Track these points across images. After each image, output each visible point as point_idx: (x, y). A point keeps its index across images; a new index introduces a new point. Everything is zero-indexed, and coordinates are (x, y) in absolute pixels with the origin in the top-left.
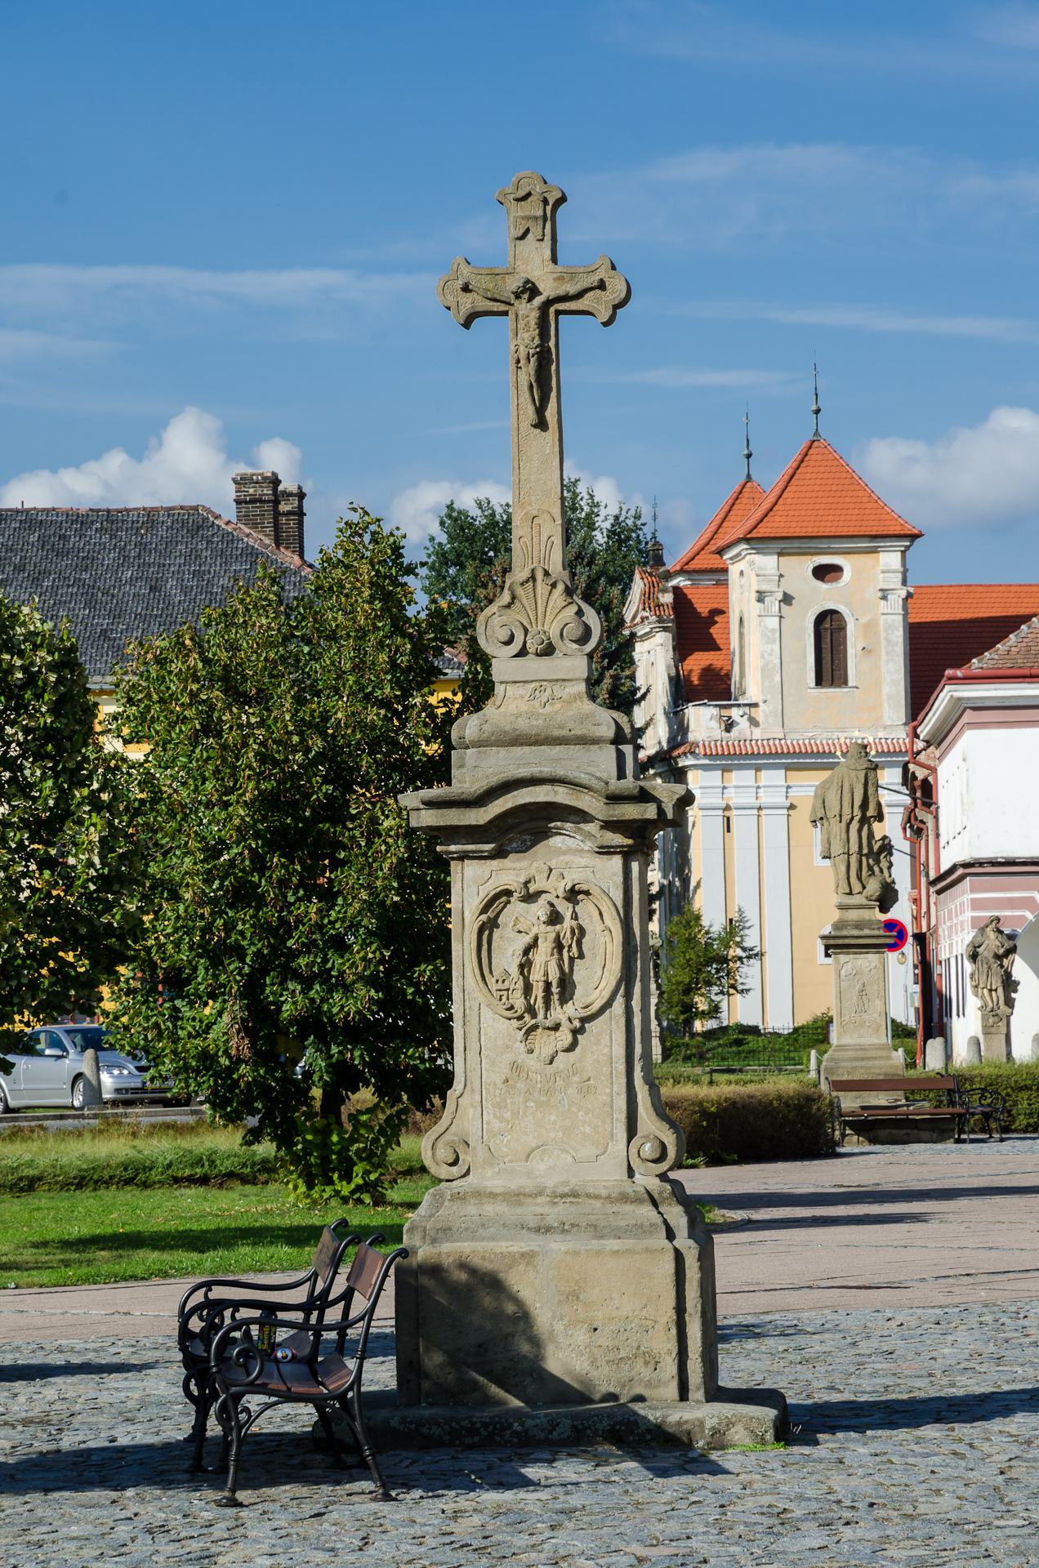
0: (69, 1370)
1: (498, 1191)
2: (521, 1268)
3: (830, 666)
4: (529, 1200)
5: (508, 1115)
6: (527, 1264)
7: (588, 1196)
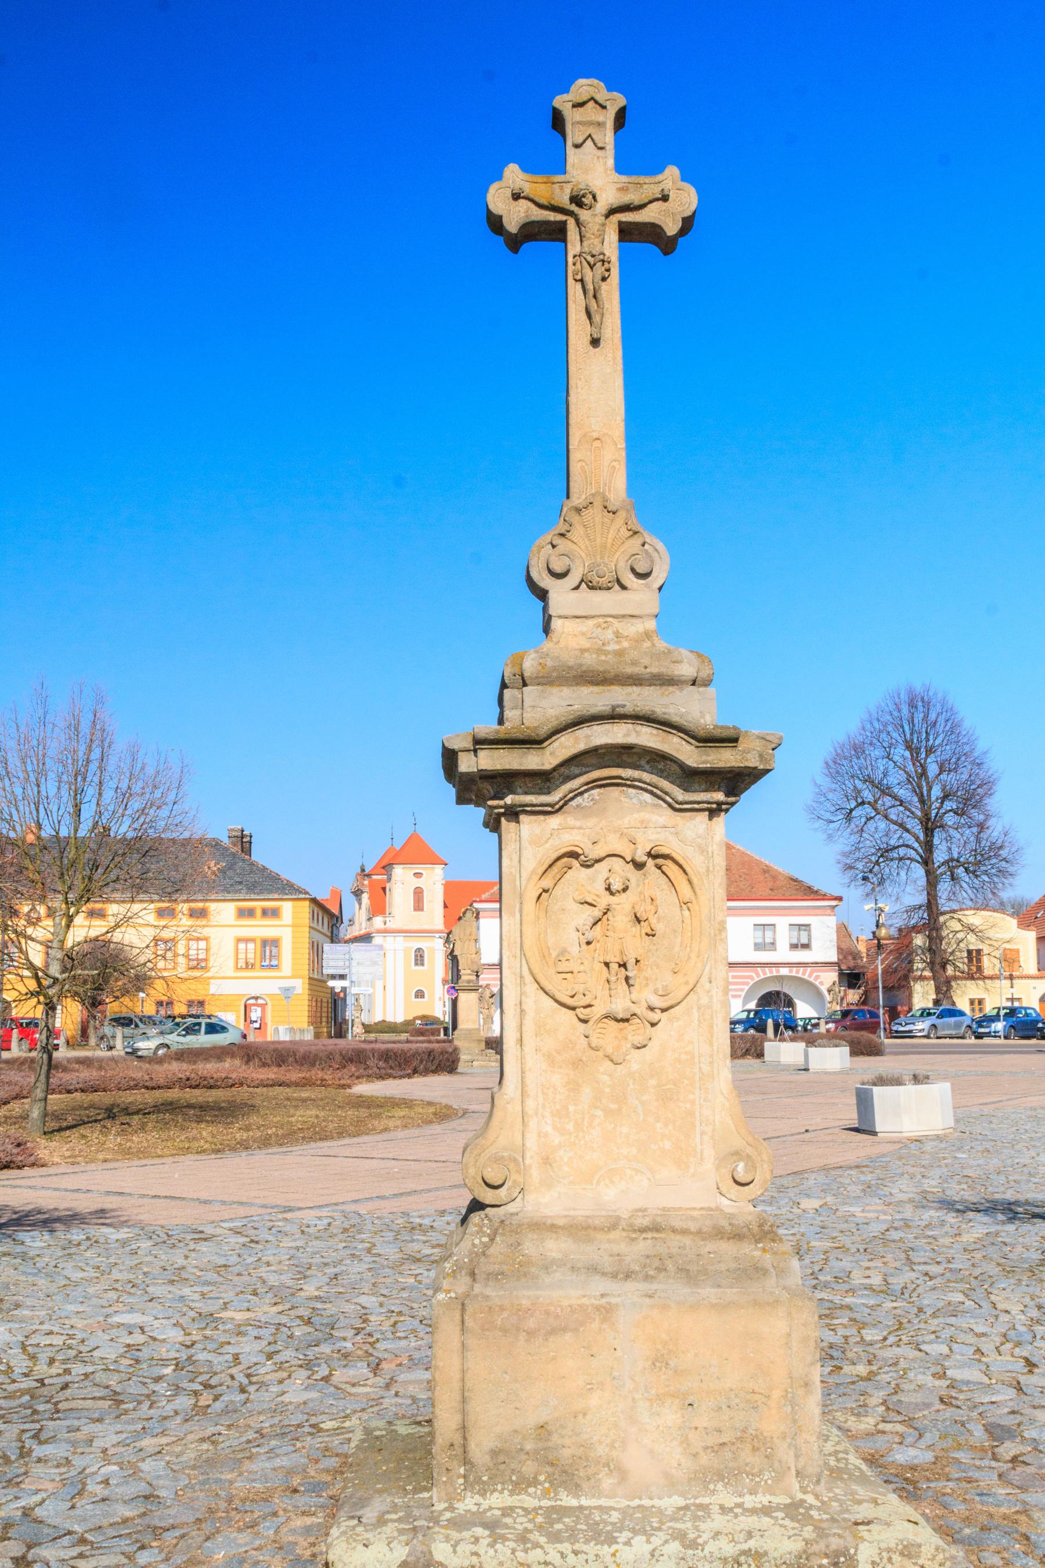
0: (651, 202)
1: (561, 1222)
2: (595, 1325)
3: (419, 906)
4: (600, 1236)
5: (570, 1126)
6: (604, 1320)
7: (674, 1231)
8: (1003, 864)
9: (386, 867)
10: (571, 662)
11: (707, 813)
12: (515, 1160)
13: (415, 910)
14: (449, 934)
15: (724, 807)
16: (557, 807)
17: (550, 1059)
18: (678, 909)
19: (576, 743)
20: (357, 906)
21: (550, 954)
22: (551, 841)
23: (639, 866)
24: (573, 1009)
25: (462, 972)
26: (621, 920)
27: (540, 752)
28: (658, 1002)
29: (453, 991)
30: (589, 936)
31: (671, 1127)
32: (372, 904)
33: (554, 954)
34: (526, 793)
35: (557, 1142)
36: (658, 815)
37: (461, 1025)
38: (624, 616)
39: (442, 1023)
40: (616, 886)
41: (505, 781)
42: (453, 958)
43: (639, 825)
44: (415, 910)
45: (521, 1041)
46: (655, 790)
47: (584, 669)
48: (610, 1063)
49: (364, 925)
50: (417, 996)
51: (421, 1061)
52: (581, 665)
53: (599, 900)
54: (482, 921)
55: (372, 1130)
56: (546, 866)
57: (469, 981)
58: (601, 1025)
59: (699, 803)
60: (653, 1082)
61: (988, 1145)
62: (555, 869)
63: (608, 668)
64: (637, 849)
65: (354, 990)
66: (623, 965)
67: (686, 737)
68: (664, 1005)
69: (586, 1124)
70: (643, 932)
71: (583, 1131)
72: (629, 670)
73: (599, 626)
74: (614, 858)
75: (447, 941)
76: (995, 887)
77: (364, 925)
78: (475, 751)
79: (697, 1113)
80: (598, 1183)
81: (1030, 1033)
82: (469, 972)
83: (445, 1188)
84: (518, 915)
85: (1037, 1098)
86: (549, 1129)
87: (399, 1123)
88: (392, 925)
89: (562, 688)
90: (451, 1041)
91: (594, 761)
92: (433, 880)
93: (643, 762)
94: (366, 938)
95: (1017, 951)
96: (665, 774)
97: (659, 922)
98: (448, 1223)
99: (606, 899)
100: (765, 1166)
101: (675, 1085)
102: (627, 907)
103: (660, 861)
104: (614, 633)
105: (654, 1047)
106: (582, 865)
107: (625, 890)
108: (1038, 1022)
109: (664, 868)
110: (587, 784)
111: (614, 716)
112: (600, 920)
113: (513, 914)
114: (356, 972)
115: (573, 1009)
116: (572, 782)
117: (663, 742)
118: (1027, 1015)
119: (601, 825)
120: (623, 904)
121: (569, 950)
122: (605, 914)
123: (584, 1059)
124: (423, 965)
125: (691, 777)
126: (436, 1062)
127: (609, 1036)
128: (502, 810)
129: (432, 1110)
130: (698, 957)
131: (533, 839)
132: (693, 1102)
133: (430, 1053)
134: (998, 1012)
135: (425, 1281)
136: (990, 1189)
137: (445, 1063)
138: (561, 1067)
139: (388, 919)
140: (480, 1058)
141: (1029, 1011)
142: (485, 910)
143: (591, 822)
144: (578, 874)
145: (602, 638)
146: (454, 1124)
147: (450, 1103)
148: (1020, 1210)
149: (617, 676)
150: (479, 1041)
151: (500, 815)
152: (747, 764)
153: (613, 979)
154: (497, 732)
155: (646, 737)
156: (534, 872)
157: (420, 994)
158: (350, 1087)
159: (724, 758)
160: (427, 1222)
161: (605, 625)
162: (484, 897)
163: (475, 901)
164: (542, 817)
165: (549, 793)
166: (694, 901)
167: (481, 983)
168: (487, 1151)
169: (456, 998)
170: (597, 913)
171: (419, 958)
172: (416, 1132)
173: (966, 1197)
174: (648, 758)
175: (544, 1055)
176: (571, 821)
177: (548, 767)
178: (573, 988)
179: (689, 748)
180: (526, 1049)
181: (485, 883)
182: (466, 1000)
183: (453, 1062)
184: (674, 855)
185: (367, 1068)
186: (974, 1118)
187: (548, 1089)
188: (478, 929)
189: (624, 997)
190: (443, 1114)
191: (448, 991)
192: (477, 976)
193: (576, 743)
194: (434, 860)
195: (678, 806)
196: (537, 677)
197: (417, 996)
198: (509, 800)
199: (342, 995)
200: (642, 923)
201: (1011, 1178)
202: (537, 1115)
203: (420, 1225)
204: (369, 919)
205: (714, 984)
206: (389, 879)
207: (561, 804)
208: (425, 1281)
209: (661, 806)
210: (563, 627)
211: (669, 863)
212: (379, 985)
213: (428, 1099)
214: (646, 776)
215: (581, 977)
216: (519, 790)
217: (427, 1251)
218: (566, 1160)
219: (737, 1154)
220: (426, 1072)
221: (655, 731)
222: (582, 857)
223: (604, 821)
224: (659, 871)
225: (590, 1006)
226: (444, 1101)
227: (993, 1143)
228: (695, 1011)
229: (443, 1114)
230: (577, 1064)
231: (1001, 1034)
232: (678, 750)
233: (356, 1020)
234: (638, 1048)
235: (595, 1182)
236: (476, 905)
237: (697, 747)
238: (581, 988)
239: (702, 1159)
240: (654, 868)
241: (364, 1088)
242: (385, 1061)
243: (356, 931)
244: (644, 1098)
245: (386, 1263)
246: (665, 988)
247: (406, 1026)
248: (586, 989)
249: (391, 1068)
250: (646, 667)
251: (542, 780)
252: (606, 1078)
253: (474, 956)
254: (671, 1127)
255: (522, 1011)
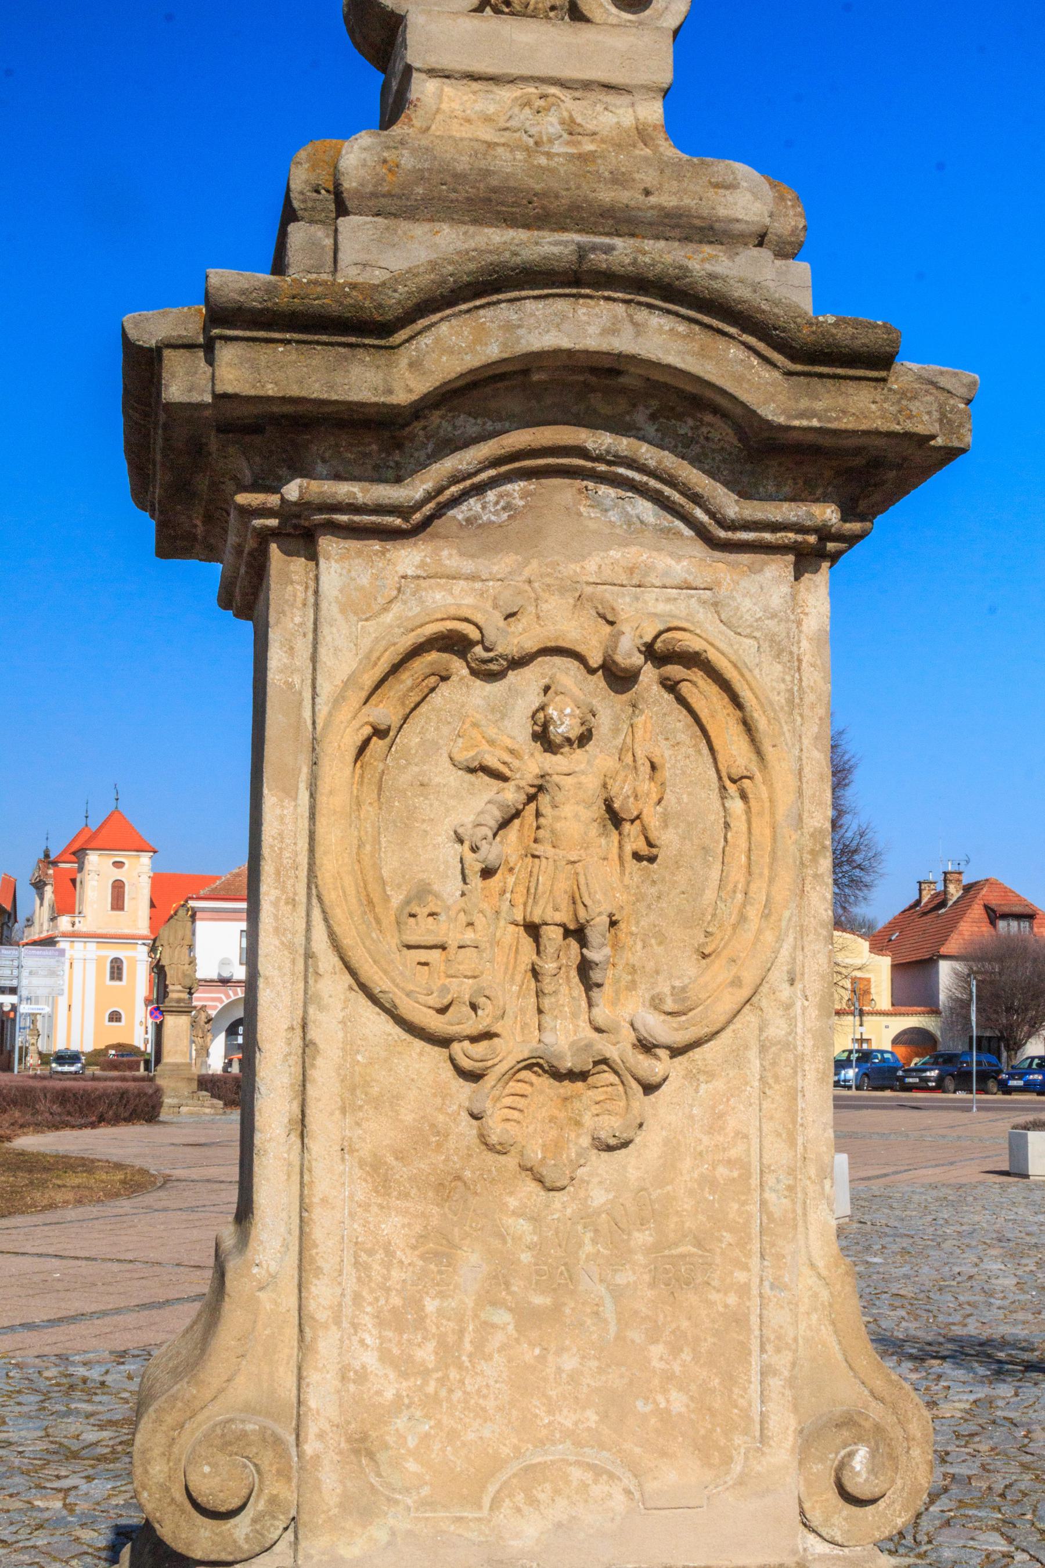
3: (118, 902)
5: (426, 1354)
8: (857, 872)
9: (79, 854)
10: (463, 164)
11: (791, 558)
12: (278, 1441)
13: (113, 909)
14: (155, 941)
15: (831, 546)
16: (417, 517)
17: (379, 1174)
18: (715, 795)
19: (477, 341)
20: (38, 902)
21: (387, 899)
22: (396, 608)
23: (619, 678)
24: (443, 1042)
25: (171, 988)
26: (573, 816)
27: (382, 358)
28: (660, 1028)
29: (157, 1013)
30: (491, 852)
31: (686, 1356)
32: (56, 901)
33: (397, 899)
34: (338, 477)
35: (389, 1395)
36: (671, 555)
37: (168, 1058)
38: (587, 85)
39: (143, 1053)
40: (565, 726)
41: (290, 432)
42: (159, 971)
43: (623, 579)
44: (113, 909)
45: (301, 1124)
46: (667, 491)
47: (494, 182)
48: (533, 1186)
49: (45, 927)
50: (111, 1019)
51: (110, 1106)
52: (487, 173)
53: (515, 763)
54: (199, 924)
55: (30, 1207)
56: (383, 666)
57: (179, 1001)
58: (514, 1086)
59: (774, 527)
60: (642, 1238)
61: (905, 1243)
62: (407, 678)
63: (555, 185)
64: (617, 636)
65: (24, 1008)
66: (578, 933)
67: (761, 346)
68: (679, 1038)
69: (468, 1347)
70: (628, 849)
71: (460, 1367)
72: (606, 195)
73: (528, 104)
74: (557, 660)
75: (153, 949)
76: (846, 901)
77: (45, 927)
78: (209, 348)
79: (754, 1320)
80: (496, 1504)
81: (886, 1083)
82: (179, 988)
83: (128, 1309)
84: (304, 796)
85: (930, 1171)
86: (370, 1359)
87: (70, 1196)
88: (81, 927)
89: (437, 226)
90: (151, 1079)
91: (513, 404)
92: (138, 872)
93: (640, 417)
94: (49, 942)
95: (868, 980)
96: (696, 449)
97: (665, 824)
98: (130, 1378)
99: (534, 763)
100: (916, 1452)
101: (699, 1244)
102: (591, 783)
103: (674, 670)
104: (562, 122)
105: (649, 1146)
106: (474, 673)
107: (584, 739)
108: (896, 1069)
109: (685, 688)
110: (496, 462)
111: (578, 279)
112: (517, 814)
113: (291, 793)
114: (28, 984)
115: (443, 1042)
116: (458, 455)
117: (703, 353)
118: (883, 1060)
119: (527, 573)
120: (581, 774)
121: (436, 887)
122: (531, 798)
123: (468, 1174)
124: (120, 979)
125: (763, 455)
126: (131, 1107)
127: (532, 1116)
128: (273, 522)
129: (120, 1176)
130: (766, 916)
131: (344, 607)
132: (743, 1290)
133: (123, 1094)
134: (849, 1057)
135: (83, 1506)
136: (941, 1318)
137: (141, 1107)
138: (406, 1196)
139: (77, 920)
140: (190, 1102)
141: (886, 1056)
142: (203, 910)
143: (502, 564)
144: (465, 695)
145: (533, 131)
146: (149, 1199)
147: (146, 1166)
148: (1001, 1355)
149: (575, 208)
150: (190, 1080)
151: (265, 536)
152: (910, 426)
153: (549, 966)
154: (271, 290)
155: (659, 339)
156: (351, 681)
157: (115, 1017)
158: (9, 1139)
159: (853, 408)
160: (94, 1374)
161: (542, 103)
162: (202, 893)
163: (192, 898)
164: (376, 546)
165: (398, 480)
166: (758, 776)
167: (195, 1003)
168: (200, 1417)
169: (162, 1022)
170: (511, 795)
171: (116, 970)
172: (94, 1210)
173: (912, 1332)
174: (655, 404)
175: (362, 1163)
176: (450, 558)
177: (401, 397)
178: (444, 989)
179: (768, 374)
180: (316, 1146)
181: (204, 877)
182: (176, 1025)
183: (153, 1107)
184: (713, 655)
185: (36, 1112)
186: (865, 1200)
187: (371, 1253)
188: (194, 934)
189: (575, 1015)
190: (136, 1182)
191: (151, 1014)
192: (191, 994)
193: (477, 341)
194: (141, 848)
195: (722, 534)
196: (374, 195)
197: (111, 1019)
198: (293, 490)
199: (12, 1015)
200: (627, 827)
201: (961, 1298)
202: (338, 1323)
203: (85, 1381)
204: (53, 919)
205: (799, 986)
206: (81, 869)
207: (428, 509)
208: (83, 1506)
209: (679, 534)
210: (440, 97)
211: (697, 675)
212: (62, 1002)
213: (115, 1159)
214: (647, 453)
215: (467, 961)
216: (321, 468)
217: (91, 1436)
218: (412, 1442)
219: (849, 1423)
220: (116, 1120)
221: (682, 328)
222: (478, 650)
223: (535, 563)
224: (669, 697)
225: (488, 1035)
226: (138, 1163)
227: (911, 1241)
228: (753, 1054)
229: (136, 1182)
230: (448, 1187)
231: (852, 1083)
232: (740, 379)
233: (31, 1048)
234: (610, 1148)
235: (486, 1501)
236: (192, 904)
237: (790, 374)
238: (465, 989)
239: (763, 1438)
240: (656, 688)
241: (29, 1142)
242: (61, 1104)
243: (35, 933)
244: (621, 1279)
245: (17, 1462)
246: (680, 993)
247: (97, 1057)
248: (480, 991)
249: (69, 1113)
250: (647, 193)
251: (383, 436)
252: (522, 1226)
253: (187, 967)
254: (686, 1356)
255: (307, 1044)
